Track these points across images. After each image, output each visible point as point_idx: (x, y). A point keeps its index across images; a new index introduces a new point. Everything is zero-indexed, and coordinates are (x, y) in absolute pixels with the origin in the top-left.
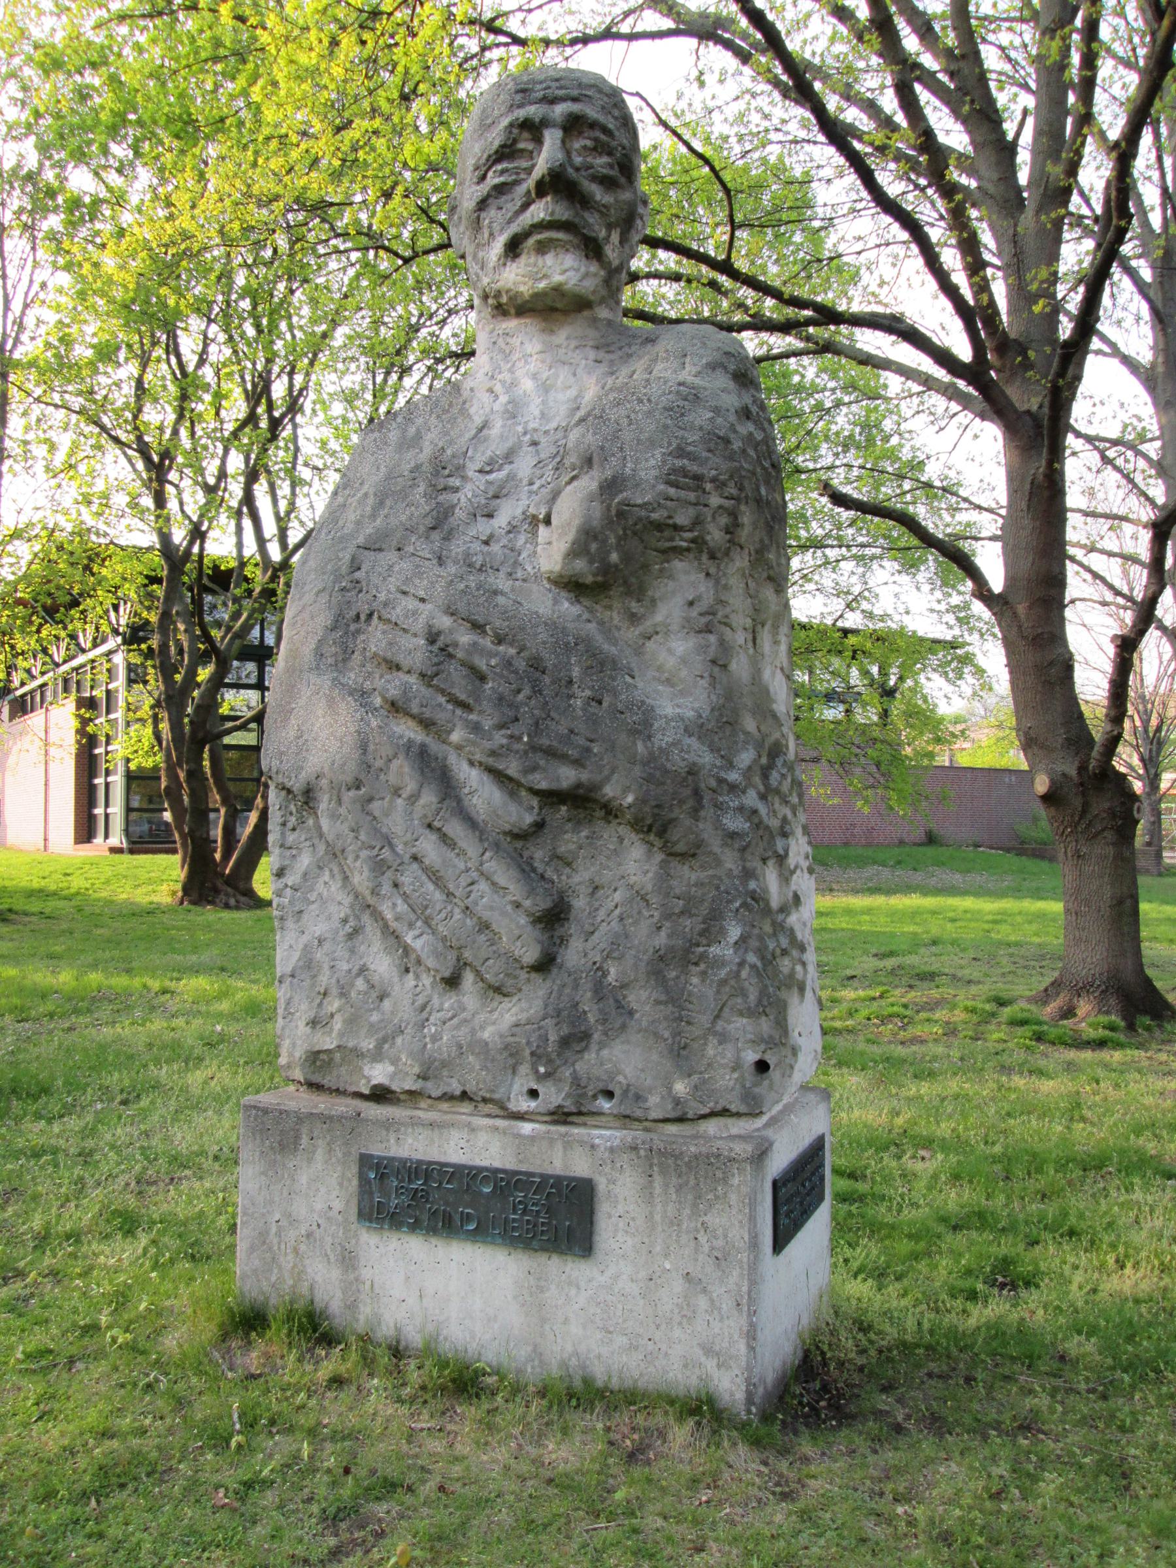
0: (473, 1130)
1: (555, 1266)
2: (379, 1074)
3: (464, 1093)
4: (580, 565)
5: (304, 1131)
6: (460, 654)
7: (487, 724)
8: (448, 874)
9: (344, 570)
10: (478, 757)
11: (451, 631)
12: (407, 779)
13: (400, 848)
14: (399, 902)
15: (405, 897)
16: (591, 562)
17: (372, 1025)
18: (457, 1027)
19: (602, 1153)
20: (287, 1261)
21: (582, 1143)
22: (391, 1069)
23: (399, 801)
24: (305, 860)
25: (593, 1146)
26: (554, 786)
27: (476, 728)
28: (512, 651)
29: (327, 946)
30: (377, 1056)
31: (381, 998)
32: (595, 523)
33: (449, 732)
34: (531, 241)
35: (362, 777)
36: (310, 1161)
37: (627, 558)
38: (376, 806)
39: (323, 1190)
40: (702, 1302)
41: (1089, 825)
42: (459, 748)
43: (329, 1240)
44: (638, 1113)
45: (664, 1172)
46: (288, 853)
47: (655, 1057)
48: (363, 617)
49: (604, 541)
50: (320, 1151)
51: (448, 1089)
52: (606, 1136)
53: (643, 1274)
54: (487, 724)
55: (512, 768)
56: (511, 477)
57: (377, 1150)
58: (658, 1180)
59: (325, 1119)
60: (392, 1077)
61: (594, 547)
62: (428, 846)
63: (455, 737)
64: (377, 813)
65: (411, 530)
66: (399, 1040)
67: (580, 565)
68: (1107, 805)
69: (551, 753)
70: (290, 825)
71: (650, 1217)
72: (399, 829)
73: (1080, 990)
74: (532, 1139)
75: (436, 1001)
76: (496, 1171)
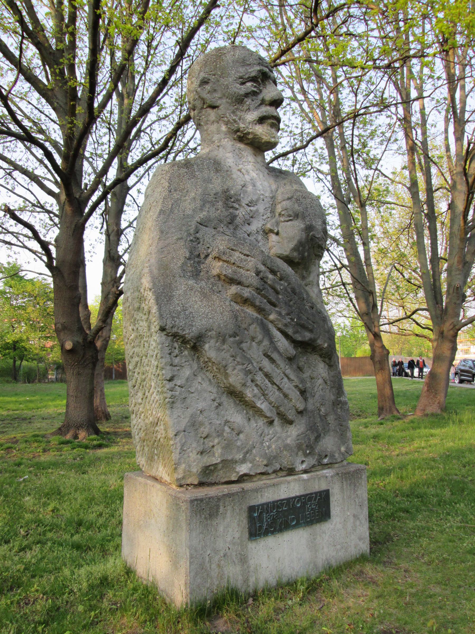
0: (289, 482)
1: (319, 528)
2: (244, 469)
3: (281, 469)
4: (295, 254)
5: (221, 504)
6: (269, 282)
7: (284, 313)
8: (274, 375)
9: (192, 231)
10: (280, 326)
11: (265, 272)
12: (258, 333)
13: (255, 364)
14: (255, 388)
15: (257, 385)
16: (299, 254)
17: (238, 447)
18: (277, 441)
19: (329, 479)
20: (214, 573)
21: (323, 476)
22: (250, 465)
23: (254, 343)
24: (187, 372)
25: (326, 477)
26: (304, 340)
27: (280, 314)
28: (286, 284)
29: (205, 414)
30: (243, 461)
31: (238, 434)
32: (303, 240)
33: (269, 315)
34: (270, 121)
35: (237, 331)
36: (224, 518)
37: (309, 255)
38: (244, 345)
39: (230, 530)
40: (358, 523)
41: (85, 361)
42: (272, 322)
43: (234, 554)
44: (334, 461)
45: (346, 480)
46: (175, 368)
47: (336, 439)
48: (202, 256)
49: (304, 247)
50: (229, 512)
51: (275, 468)
52: (328, 472)
53: (343, 520)
54: (284, 313)
55: (290, 331)
56: (257, 211)
57: (253, 503)
58: (345, 483)
59: (229, 495)
60: (250, 469)
61: (301, 248)
62: (266, 363)
63: (272, 317)
64: (245, 349)
65: (221, 221)
66: (254, 451)
67: (295, 254)
68: (91, 354)
69: (303, 327)
70: (175, 354)
71: (343, 498)
72: (255, 356)
73: (79, 427)
74: (308, 480)
75: (266, 431)
76: (300, 497)
